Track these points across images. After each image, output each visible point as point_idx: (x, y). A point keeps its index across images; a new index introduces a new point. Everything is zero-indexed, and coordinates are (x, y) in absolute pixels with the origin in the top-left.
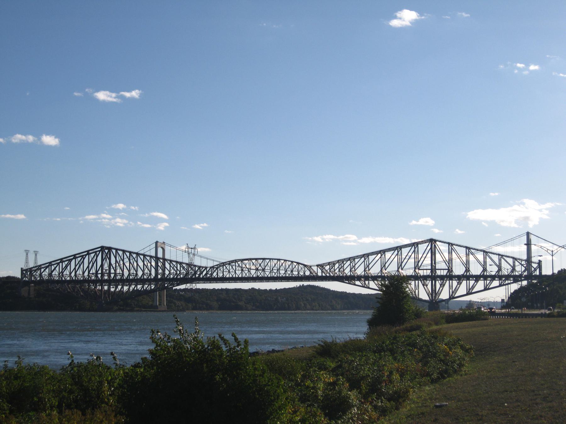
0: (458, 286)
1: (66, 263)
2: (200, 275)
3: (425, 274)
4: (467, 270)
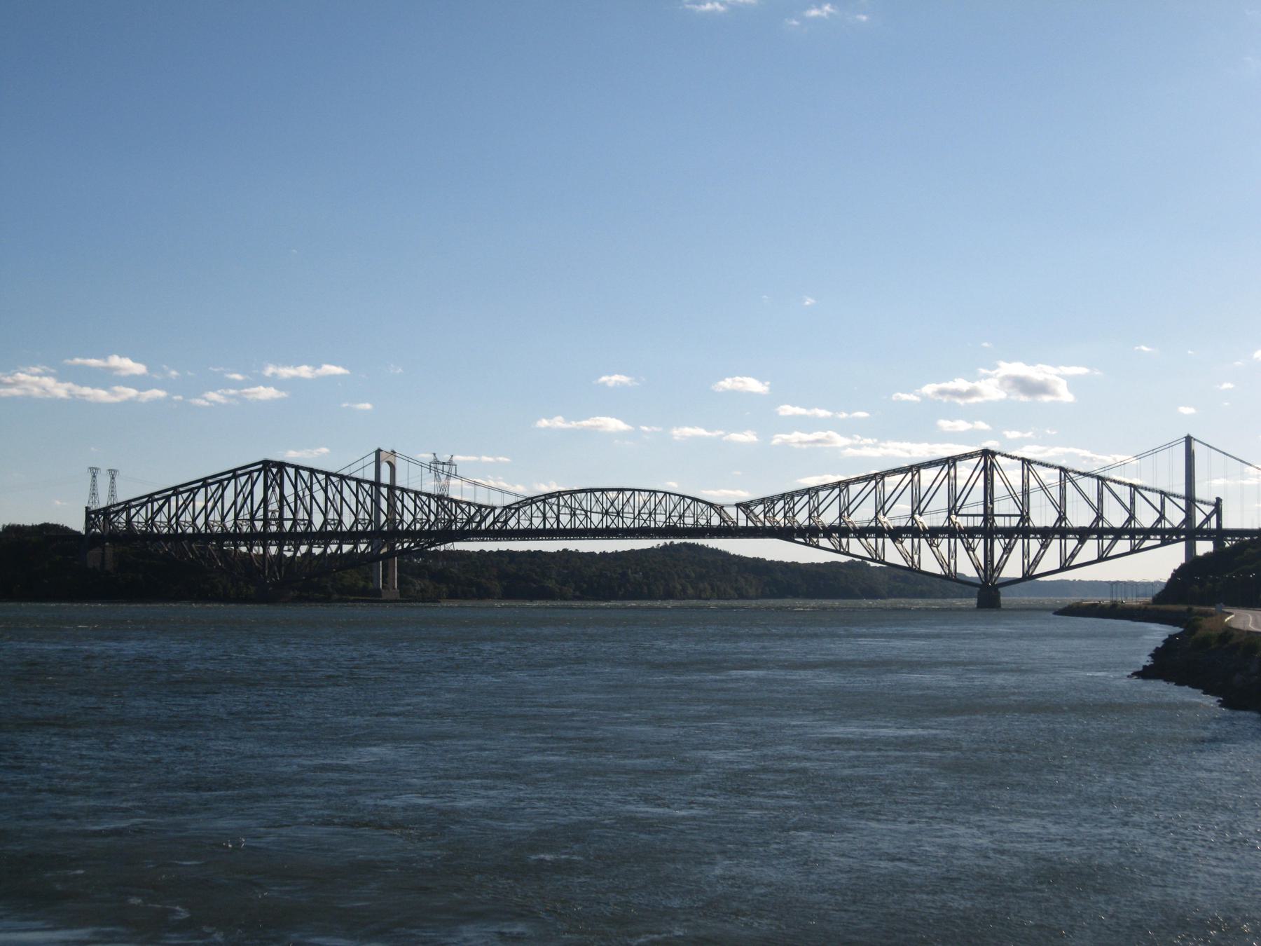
0: (1042, 551)
2: (479, 523)
3: (971, 525)
4: (1062, 517)
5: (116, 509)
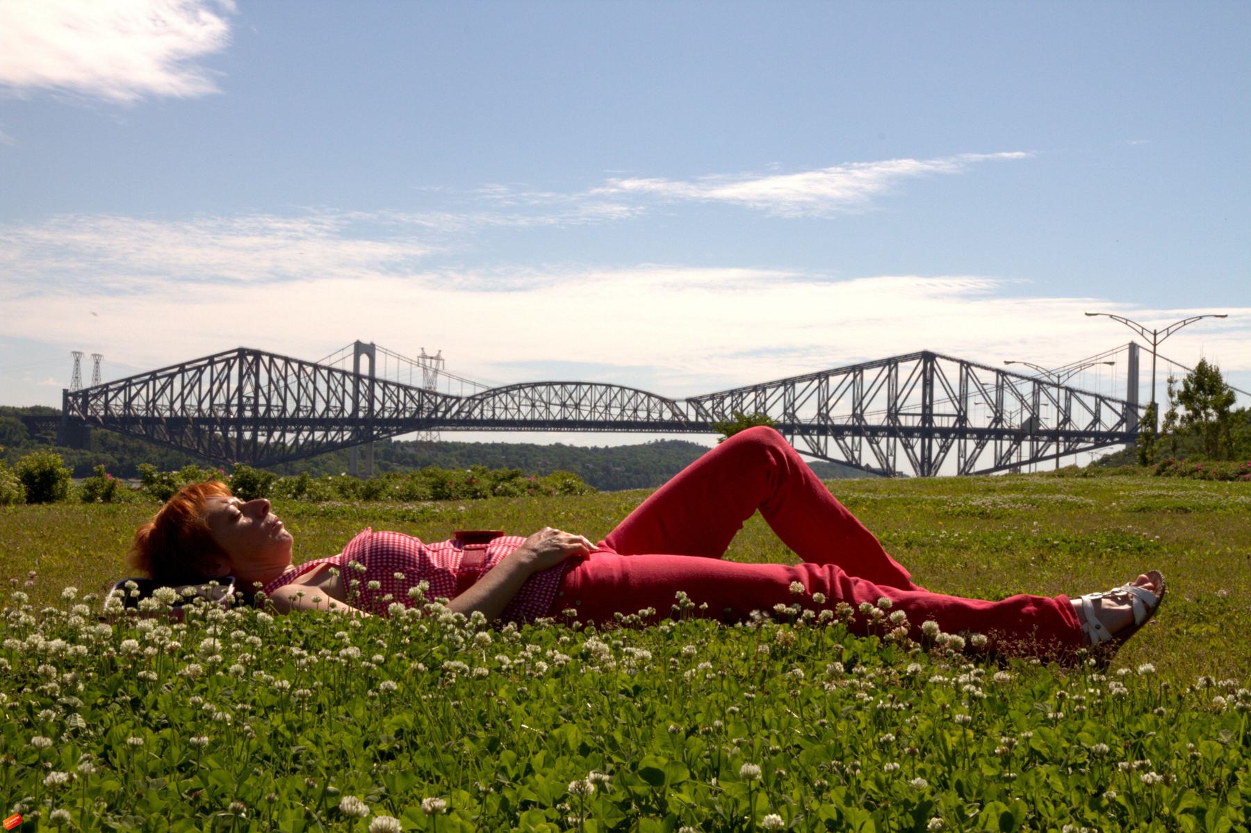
2: (445, 412)
4: (998, 419)
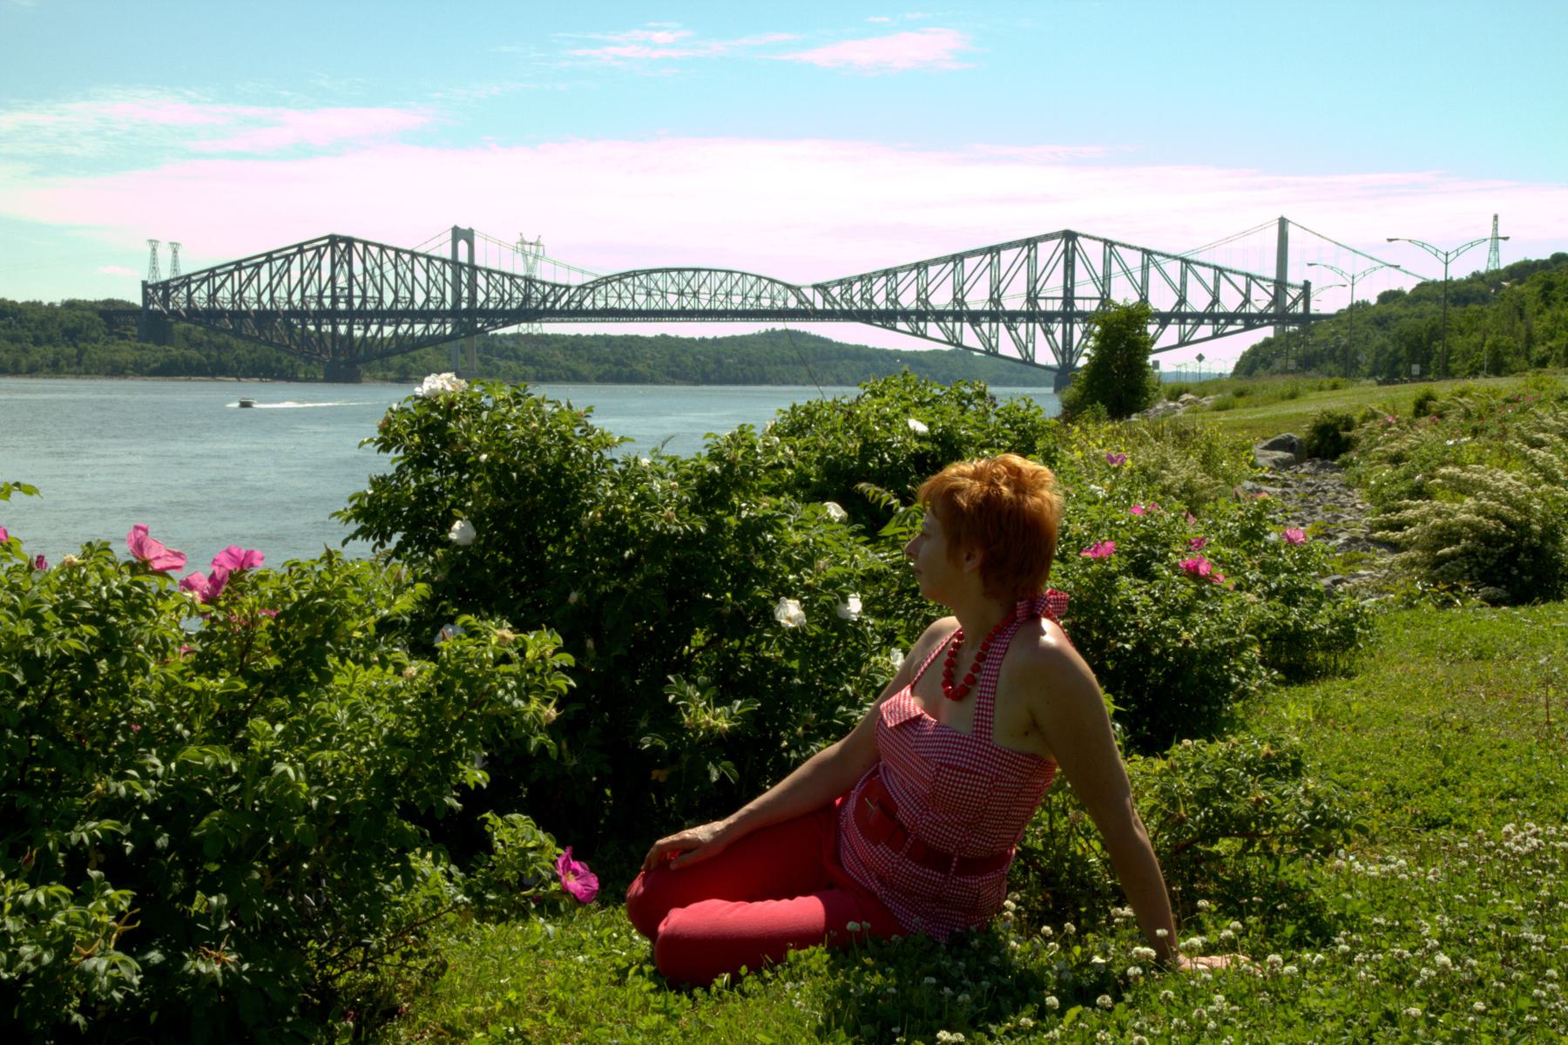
1: (249, 271)
2: (554, 302)
5: (175, 283)
